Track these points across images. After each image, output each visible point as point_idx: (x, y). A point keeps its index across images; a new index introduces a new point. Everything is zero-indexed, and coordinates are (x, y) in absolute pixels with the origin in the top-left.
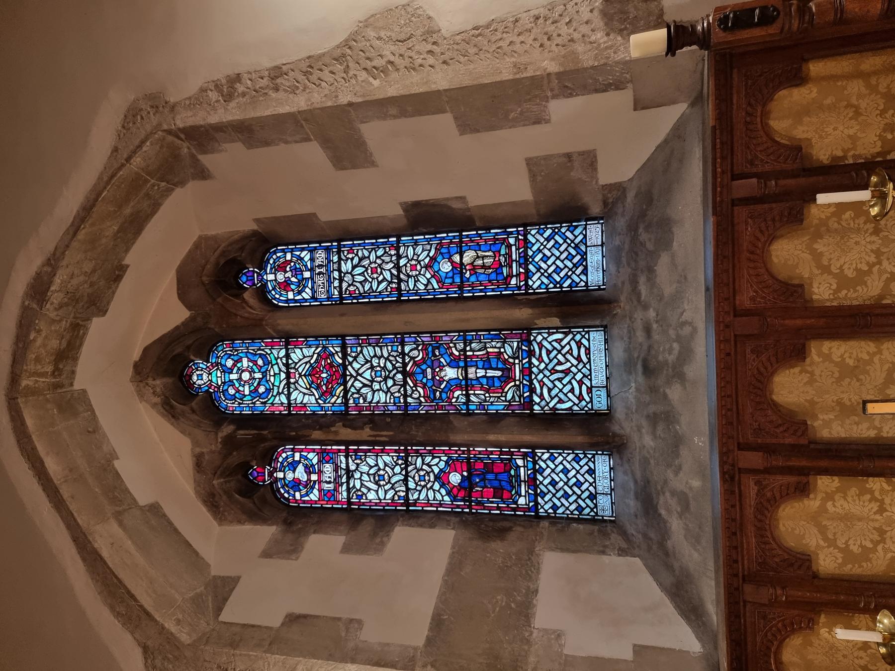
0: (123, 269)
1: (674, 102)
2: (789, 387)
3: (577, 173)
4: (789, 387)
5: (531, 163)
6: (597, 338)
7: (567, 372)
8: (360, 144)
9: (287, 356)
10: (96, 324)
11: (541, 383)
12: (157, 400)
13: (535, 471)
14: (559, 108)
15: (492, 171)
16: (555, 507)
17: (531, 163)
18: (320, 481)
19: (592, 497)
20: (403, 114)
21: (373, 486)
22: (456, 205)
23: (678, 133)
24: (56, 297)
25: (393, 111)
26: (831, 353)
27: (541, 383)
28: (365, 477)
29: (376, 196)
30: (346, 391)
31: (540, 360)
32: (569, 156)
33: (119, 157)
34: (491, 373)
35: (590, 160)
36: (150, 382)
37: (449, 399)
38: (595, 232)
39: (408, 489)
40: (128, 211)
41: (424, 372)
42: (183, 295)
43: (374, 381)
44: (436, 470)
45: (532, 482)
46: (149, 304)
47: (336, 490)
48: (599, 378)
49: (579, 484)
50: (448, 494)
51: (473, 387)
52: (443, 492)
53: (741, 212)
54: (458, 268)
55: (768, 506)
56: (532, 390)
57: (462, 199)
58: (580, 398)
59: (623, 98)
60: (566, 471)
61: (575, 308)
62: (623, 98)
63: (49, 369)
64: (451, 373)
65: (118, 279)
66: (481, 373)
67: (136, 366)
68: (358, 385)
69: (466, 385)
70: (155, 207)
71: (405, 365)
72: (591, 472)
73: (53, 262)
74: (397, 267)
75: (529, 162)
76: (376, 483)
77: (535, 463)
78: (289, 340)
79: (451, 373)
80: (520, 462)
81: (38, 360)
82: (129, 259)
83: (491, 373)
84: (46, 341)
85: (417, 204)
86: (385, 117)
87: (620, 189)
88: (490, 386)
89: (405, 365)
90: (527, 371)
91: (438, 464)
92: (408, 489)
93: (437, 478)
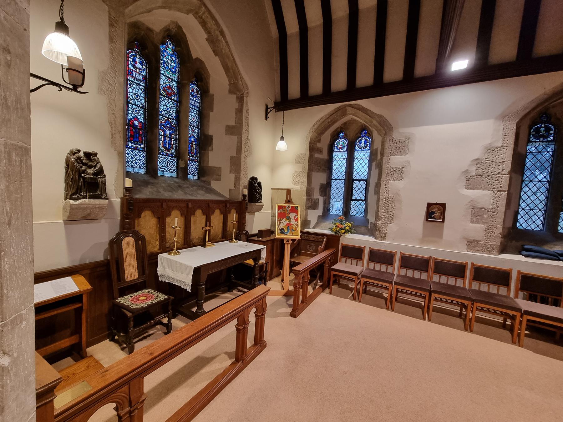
0: (216, 55)
1: (229, 195)
2: (199, 212)
3: (215, 176)
4: (199, 212)
5: (220, 168)
6: (174, 175)
7: (167, 166)
8: (232, 134)
9: (175, 81)
10: (205, 36)
11: (165, 158)
12: (171, 28)
13: (139, 150)
14: (233, 176)
15: (216, 158)
16: (128, 154)
17: (220, 168)
18: (136, 72)
19: (132, 166)
20: (238, 147)
21: (134, 92)
22: (210, 148)
23: (223, 196)
24: (220, 37)
25: (239, 145)
26: (204, 217)
27: (165, 158)
28: (137, 90)
29: (215, 129)
30: (164, 96)
31: (171, 159)
32: (220, 176)
33: (242, 78)
34: (167, 144)
35: (219, 180)
36: (176, 29)
37: (161, 129)
38: (196, 178)
39: (133, 105)
40: (231, 71)
41: (168, 124)
42: (197, 59)
43: (167, 106)
44: (139, 117)
45: (136, 149)
46: (199, 46)
47: (132, 76)
48: (165, 174)
49: (136, 163)
50: (131, 119)
51: (164, 138)
52: (131, 117)
53: (224, 205)
54: (192, 143)
55: (180, 209)
56: (163, 155)
57: (212, 150)
58: (161, 168)
59: (232, 187)
60: (140, 160)
61: (182, 172)
62: (232, 187)
63: (203, 17)
64: (168, 132)
65: (214, 51)
66: (168, 141)
67: (181, 28)
68: (166, 101)
69: (164, 136)
70: (228, 76)
71: (171, 119)
72: (140, 167)
73: (229, 48)
74: (194, 126)
75: (220, 168)
76: (135, 94)
77: (142, 151)
78: (179, 83)
79: (168, 132)
80: (142, 146)
81: (207, 17)
82: (217, 57)
83: (167, 144)
84: (210, 24)
85: (212, 139)
86: (238, 142)
87: (209, 184)
88: (164, 144)
89: (171, 119)
90: (167, 155)
91: (141, 118)
92: (133, 105)
93: (136, 117)
